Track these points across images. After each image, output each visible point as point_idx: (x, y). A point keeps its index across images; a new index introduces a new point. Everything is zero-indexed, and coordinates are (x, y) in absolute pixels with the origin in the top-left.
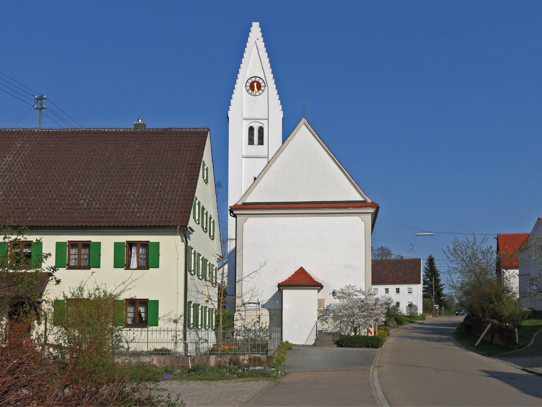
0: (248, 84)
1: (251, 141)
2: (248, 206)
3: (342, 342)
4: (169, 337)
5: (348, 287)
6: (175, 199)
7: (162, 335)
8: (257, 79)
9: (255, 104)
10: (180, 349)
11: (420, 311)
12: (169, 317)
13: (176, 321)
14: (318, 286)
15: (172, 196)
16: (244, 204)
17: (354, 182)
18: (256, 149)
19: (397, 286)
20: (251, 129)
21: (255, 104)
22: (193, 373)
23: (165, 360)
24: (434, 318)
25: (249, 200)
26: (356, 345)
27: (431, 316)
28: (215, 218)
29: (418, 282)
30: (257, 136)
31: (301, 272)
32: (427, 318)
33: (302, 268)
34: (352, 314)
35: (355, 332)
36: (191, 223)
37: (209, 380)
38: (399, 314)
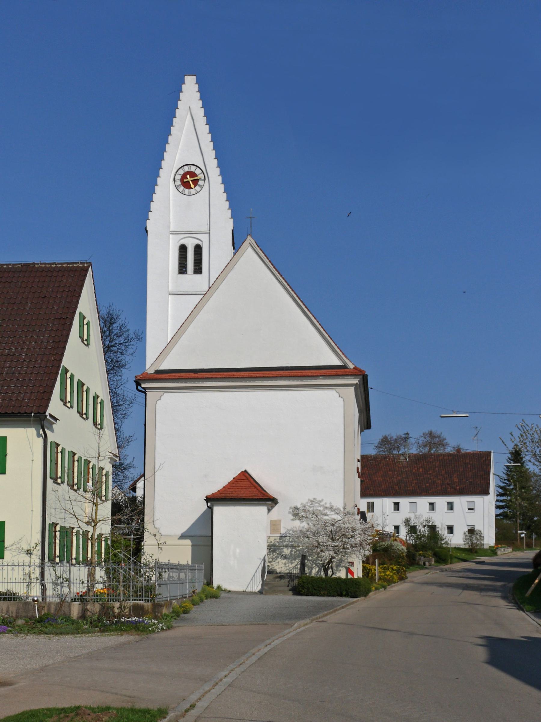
0: (178, 177)
1: (182, 269)
2: (164, 376)
3: (302, 585)
4: (19, 574)
5: (311, 501)
6: (31, 373)
7: (15, 572)
8: (193, 169)
9: (188, 210)
10: (36, 592)
11: (489, 539)
12: (18, 546)
13: (29, 552)
14: (269, 501)
15: (28, 367)
16: (158, 372)
17: (326, 336)
18: (191, 280)
19: (396, 500)
20: (183, 249)
21: (188, 210)
22: (39, 625)
23: (8, 608)
24: (514, 553)
25: (165, 366)
26: (322, 593)
27: (510, 550)
28: (104, 395)
29: (486, 492)
30: (190, 259)
31: (245, 477)
32: (499, 552)
33: (246, 471)
34: (316, 544)
35: (326, 571)
36: (55, 407)
37: (57, 634)
38: (444, 546)
